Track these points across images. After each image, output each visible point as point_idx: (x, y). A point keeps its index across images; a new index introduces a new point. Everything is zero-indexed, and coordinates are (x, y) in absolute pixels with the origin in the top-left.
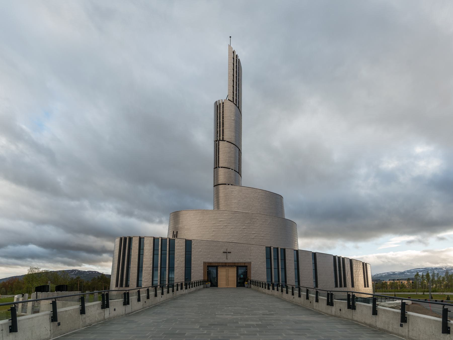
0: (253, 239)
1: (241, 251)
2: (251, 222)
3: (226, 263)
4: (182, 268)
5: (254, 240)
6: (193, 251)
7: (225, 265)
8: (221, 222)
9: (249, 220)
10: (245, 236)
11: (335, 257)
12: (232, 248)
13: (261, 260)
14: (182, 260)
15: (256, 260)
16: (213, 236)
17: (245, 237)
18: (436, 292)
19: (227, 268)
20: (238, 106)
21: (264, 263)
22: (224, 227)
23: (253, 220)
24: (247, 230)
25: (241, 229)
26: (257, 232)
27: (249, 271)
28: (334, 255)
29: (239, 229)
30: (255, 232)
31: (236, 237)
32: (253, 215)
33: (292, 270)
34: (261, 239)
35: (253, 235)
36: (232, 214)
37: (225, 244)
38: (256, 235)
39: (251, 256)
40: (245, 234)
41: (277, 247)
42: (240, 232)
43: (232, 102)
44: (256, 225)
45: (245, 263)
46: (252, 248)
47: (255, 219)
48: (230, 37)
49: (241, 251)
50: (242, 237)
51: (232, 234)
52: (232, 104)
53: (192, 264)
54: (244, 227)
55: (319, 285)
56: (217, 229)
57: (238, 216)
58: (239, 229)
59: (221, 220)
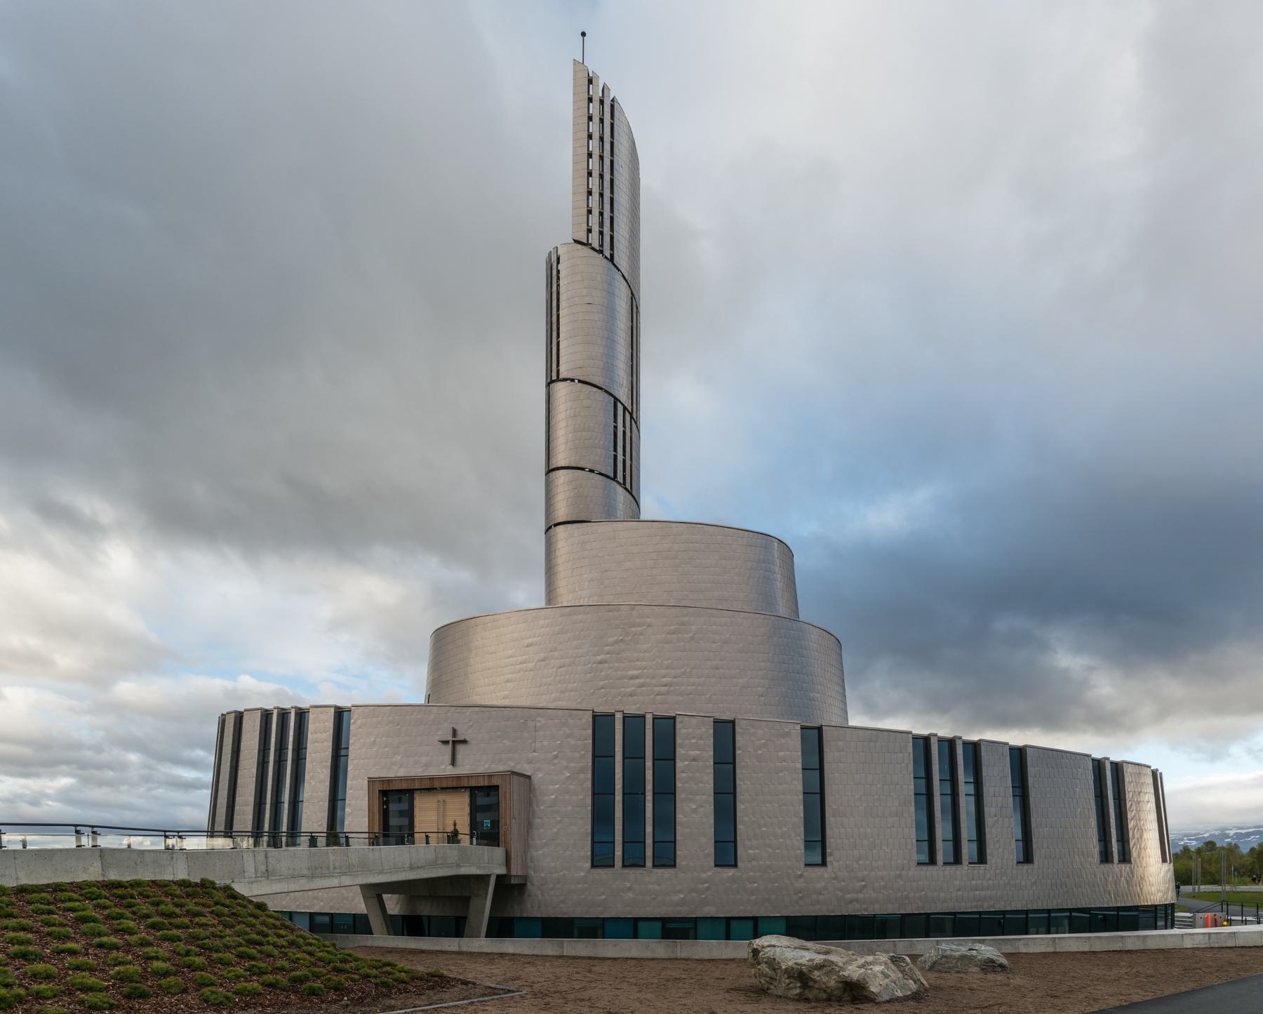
0: (631, 695)
1: (499, 733)
2: (626, 638)
3: (432, 779)
4: (321, 803)
5: (636, 698)
6: (352, 744)
7: (433, 786)
8: (531, 648)
9: (620, 630)
10: (602, 688)
11: (1098, 765)
12: (471, 726)
13: (573, 765)
14: (322, 776)
15: (554, 764)
16: (507, 698)
17: (603, 690)
18: (38, 850)
19: (441, 797)
20: (607, 253)
21: (582, 776)
22: (539, 663)
23: (634, 629)
24: (611, 665)
25: (589, 666)
26: (646, 671)
27: (503, 805)
28: (1097, 755)
29: (586, 667)
30: (640, 671)
31: (573, 693)
32: (635, 612)
33: (704, 797)
34: (658, 695)
35: (632, 681)
36: (564, 617)
37: (449, 714)
38: (642, 680)
39: (534, 751)
40: (601, 683)
41: (731, 718)
42: (589, 676)
43: (583, 247)
44: (645, 646)
45: (490, 776)
46: (539, 721)
47: (639, 626)
48: (583, 34)
49: (499, 733)
50: (593, 693)
51: (560, 685)
52: (586, 251)
53: (347, 789)
54: (599, 658)
55: (831, 854)
56: (519, 672)
57: (581, 622)
58: (585, 665)
59: (530, 640)
